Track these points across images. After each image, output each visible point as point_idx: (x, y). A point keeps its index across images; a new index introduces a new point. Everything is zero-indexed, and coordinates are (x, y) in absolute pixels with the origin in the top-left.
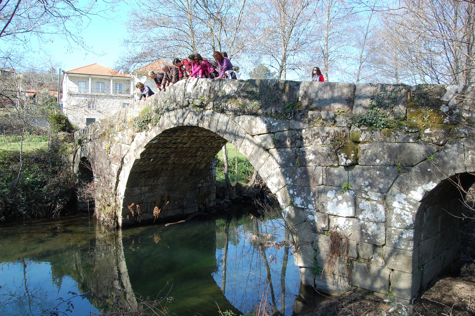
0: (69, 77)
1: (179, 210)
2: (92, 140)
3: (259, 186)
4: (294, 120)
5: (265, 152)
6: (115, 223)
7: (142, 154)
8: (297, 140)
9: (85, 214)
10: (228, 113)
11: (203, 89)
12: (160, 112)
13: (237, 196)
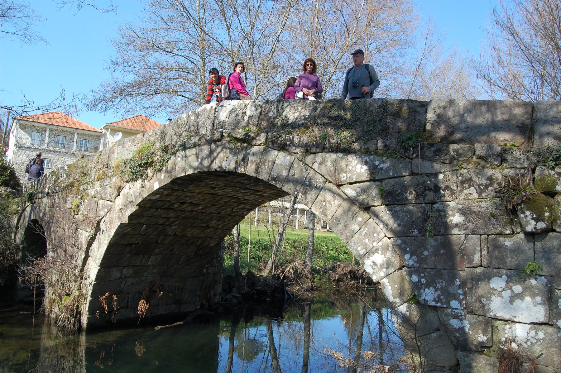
0: (20, 124)
3: (279, 277)
4: (421, 160)
5: (361, 212)
6: (77, 323)
7: (131, 217)
8: (427, 192)
10: (293, 149)
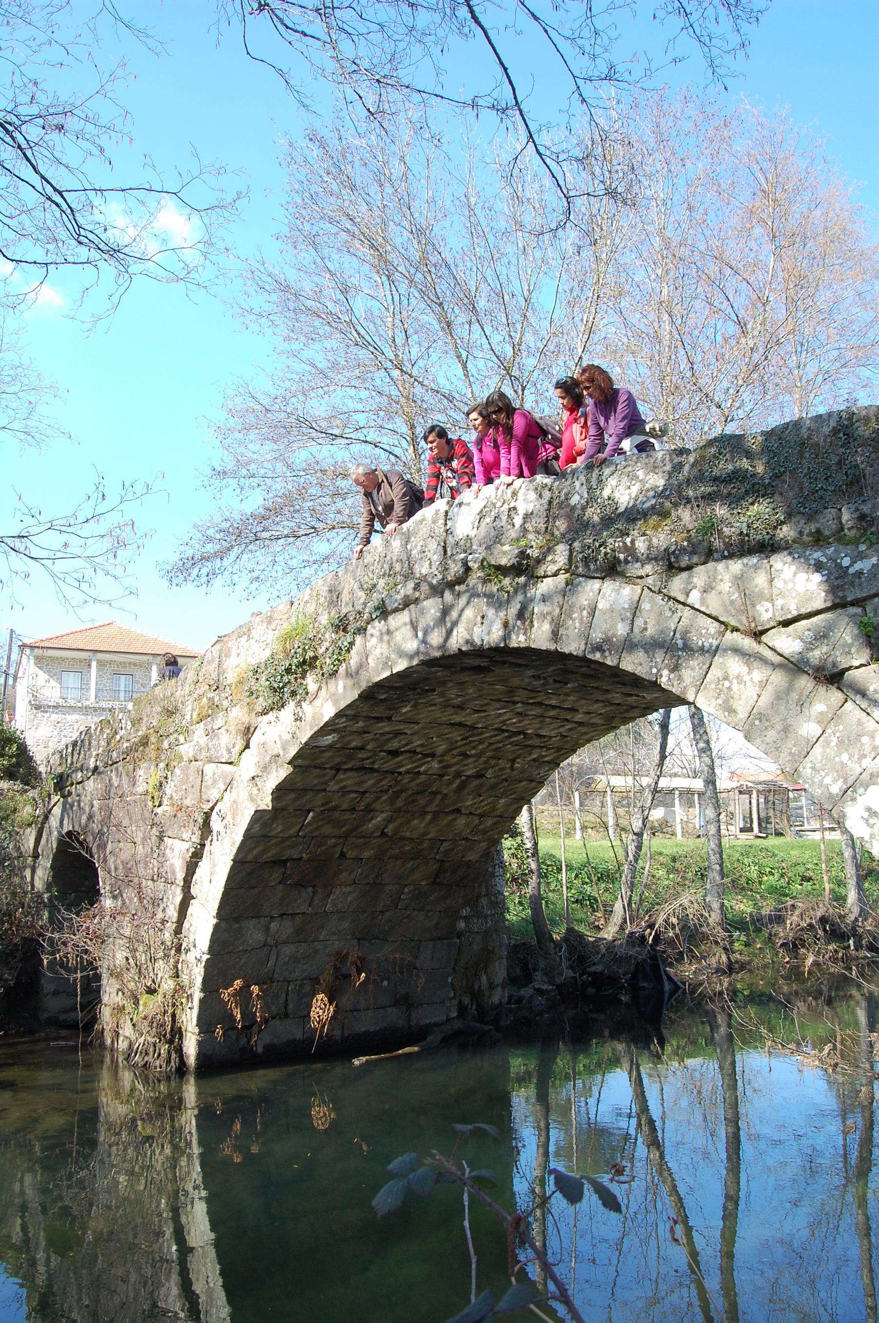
1: (395, 1010)
2: (102, 769)
3: (643, 938)
5: (822, 689)
6: (174, 1055)
7: (280, 792)
9: (64, 1032)
10: (635, 569)
11: (521, 511)
12: (351, 628)
13: (570, 974)
